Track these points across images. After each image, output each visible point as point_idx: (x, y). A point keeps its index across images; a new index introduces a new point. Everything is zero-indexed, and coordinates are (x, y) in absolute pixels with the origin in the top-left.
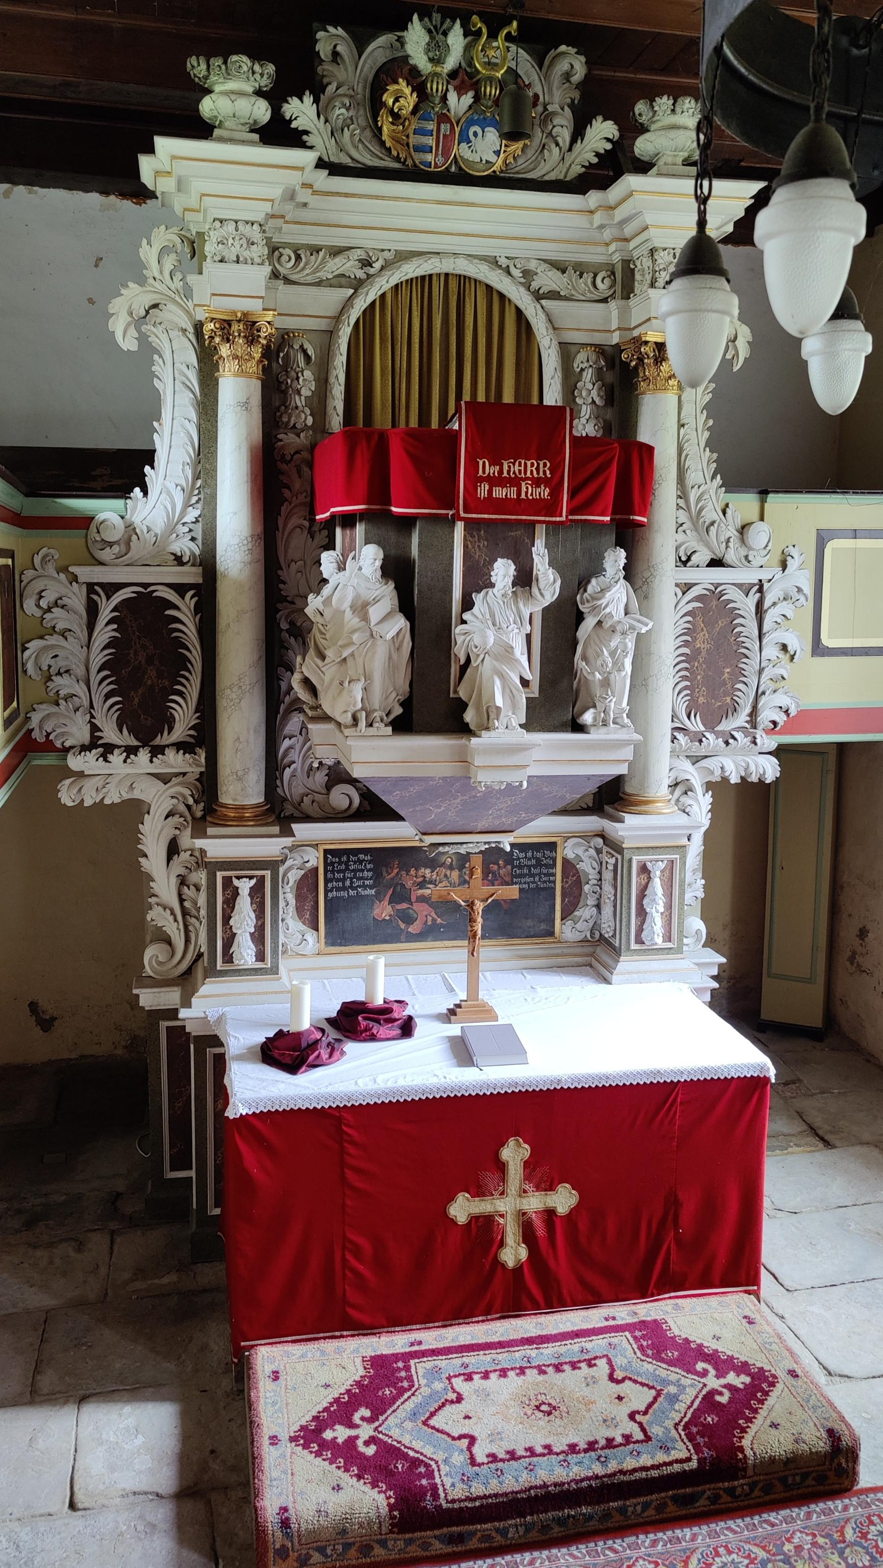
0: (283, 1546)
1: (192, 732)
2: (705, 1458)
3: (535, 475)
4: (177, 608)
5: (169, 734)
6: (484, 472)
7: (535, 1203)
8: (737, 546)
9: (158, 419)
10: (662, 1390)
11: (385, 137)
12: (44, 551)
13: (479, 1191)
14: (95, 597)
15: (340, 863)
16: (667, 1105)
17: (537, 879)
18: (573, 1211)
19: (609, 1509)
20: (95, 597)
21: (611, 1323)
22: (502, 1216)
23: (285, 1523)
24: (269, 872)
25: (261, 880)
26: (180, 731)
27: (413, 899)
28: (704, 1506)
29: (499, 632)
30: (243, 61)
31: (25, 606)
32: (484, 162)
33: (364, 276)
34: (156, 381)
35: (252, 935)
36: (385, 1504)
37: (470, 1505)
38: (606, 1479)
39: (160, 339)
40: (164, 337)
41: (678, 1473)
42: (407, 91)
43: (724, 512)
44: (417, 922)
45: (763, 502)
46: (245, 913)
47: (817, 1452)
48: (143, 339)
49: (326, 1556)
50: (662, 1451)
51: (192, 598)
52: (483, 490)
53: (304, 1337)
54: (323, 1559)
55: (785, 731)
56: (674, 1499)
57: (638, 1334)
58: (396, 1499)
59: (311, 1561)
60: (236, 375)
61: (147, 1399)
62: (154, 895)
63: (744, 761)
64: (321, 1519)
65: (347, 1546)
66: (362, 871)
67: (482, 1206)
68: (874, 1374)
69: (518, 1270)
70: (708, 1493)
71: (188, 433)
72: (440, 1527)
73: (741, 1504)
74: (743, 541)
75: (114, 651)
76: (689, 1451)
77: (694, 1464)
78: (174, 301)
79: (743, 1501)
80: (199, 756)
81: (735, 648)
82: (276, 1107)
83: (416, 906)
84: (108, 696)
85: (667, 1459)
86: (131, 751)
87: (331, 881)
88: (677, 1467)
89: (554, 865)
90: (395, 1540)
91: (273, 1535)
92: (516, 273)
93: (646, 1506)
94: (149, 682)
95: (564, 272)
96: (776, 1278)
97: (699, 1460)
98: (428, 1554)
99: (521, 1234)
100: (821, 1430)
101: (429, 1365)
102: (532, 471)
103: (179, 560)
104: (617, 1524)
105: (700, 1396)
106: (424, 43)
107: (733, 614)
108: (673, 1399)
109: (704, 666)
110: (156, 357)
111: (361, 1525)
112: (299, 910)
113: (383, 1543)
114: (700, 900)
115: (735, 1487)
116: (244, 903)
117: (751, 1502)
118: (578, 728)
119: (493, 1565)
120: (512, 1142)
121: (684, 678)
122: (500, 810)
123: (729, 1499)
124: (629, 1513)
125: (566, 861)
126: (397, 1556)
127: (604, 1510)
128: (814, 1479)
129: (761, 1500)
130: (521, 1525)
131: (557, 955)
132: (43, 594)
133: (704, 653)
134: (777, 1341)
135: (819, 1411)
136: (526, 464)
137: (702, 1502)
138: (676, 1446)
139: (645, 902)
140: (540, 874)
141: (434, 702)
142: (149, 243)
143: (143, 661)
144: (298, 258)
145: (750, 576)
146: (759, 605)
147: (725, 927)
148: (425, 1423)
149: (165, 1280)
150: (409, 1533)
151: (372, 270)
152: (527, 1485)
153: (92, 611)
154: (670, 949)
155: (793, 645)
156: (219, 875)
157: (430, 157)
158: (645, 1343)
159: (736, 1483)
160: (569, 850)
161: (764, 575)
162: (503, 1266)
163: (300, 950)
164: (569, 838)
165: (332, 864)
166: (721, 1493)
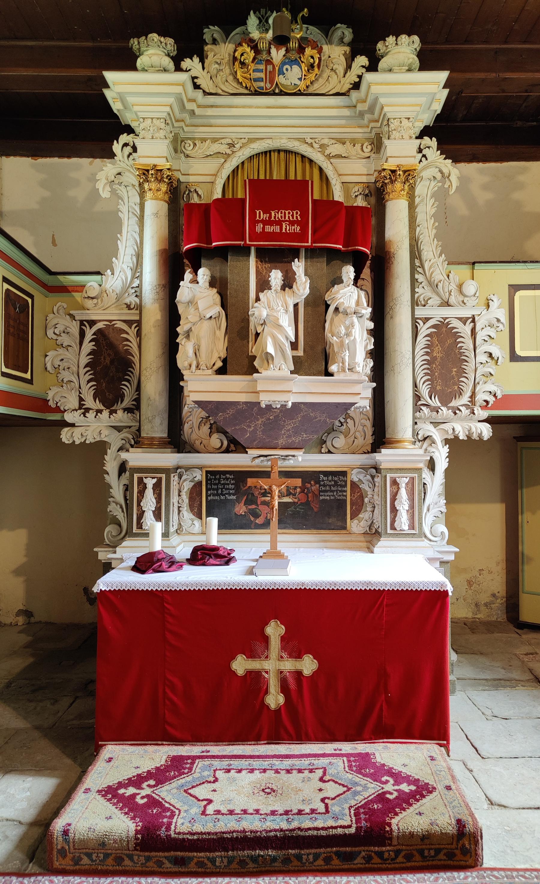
0: (63, 847)
1: (134, 403)
2: (361, 827)
3: (291, 219)
4: (127, 333)
5: (121, 403)
6: (260, 217)
7: (289, 665)
8: (456, 294)
9: (121, 233)
10: (352, 788)
11: (239, 76)
12: (59, 304)
13: (251, 655)
14: (84, 327)
15: (215, 479)
16: (377, 605)
17: (335, 493)
18: (315, 673)
19: (288, 855)
20: (84, 327)
21: (338, 752)
22: (267, 672)
23: (66, 833)
24: (164, 475)
25: (160, 480)
26: (127, 402)
27: (259, 503)
28: (362, 864)
29: (276, 313)
30: (154, 36)
31: (48, 333)
32: (293, 85)
33: (230, 153)
34: (119, 213)
35: (154, 512)
36: (134, 829)
37: (190, 837)
38: (287, 832)
39: (122, 191)
40: (124, 190)
41: (340, 835)
42: (248, 50)
43: (448, 276)
44: (261, 517)
45: (473, 269)
46: (149, 498)
47: (446, 833)
48: (113, 192)
49: (92, 860)
50: (333, 820)
51: (135, 327)
52: (259, 228)
53: (138, 742)
54: (90, 862)
55: (493, 408)
56: (337, 853)
57: (352, 759)
58: (142, 828)
59: (82, 863)
60: (152, 199)
61: (44, 775)
62: (112, 497)
63: (468, 425)
64: (89, 833)
65: (107, 856)
66: (228, 484)
67: (254, 665)
68: (524, 806)
69: (278, 711)
70: (363, 854)
71: (135, 238)
72: (169, 850)
73: (389, 866)
74: (461, 292)
75: (93, 357)
76: (352, 821)
77: (353, 830)
78: (129, 171)
79: (390, 864)
80: (136, 415)
81: (459, 356)
82: (124, 588)
83: (261, 507)
84: (89, 382)
85: (334, 824)
86: (99, 411)
87: (210, 490)
88: (340, 831)
89: (345, 486)
90: (139, 856)
91: (57, 839)
92: (316, 146)
93: (316, 857)
94: (111, 374)
95: (344, 143)
96: (477, 751)
97: (357, 828)
98: (161, 870)
99: (279, 686)
100: (453, 820)
101: (208, 763)
102: (289, 217)
103: (129, 307)
104: (296, 868)
105: (377, 793)
106: (256, 24)
107: (457, 336)
108: (356, 793)
109: (439, 367)
110: (120, 201)
111: (115, 841)
112: (191, 507)
113: (130, 857)
114: (444, 514)
115: (384, 852)
116: (149, 493)
117: (397, 866)
118: (328, 374)
119: (201, 882)
120: (273, 623)
121: (426, 374)
122: (289, 430)
123: (379, 861)
124: (304, 861)
125: (353, 483)
126: (141, 869)
127: (285, 855)
128: (445, 854)
129: (404, 865)
130: (225, 857)
131: (348, 541)
132: (56, 326)
133: (439, 359)
134: (447, 770)
135: (457, 809)
136: (285, 213)
137: (359, 860)
138: (344, 818)
139: (396, 503)
140: (337, 491)
141: (239, 359)
142: (118, 142)
143: (109, 363)
144: (195, 145)
145: (466, 313)
146: (473, 332)
147: (498, 564)
148: (186, 791)
149: (91, 721)
150: (147, 852)
151: (235, 148)
152: (232, 829)
153: (82, 335)
154: (414, 534)
155: (496, 353)
156: (136, 476)
157: (262, 84)
158: (354, 764)
159: (384, 848)
160: (354, 476)
161: (475, 312)
162: (268, 707)
163: (191, 530)
164: (354, 468)
165: (211, 479)
166: (373, 854)
